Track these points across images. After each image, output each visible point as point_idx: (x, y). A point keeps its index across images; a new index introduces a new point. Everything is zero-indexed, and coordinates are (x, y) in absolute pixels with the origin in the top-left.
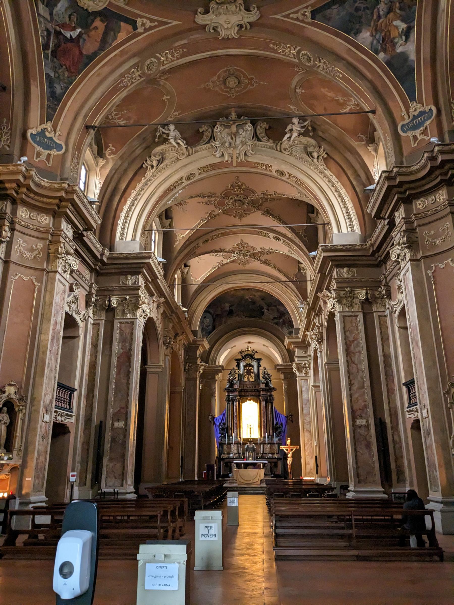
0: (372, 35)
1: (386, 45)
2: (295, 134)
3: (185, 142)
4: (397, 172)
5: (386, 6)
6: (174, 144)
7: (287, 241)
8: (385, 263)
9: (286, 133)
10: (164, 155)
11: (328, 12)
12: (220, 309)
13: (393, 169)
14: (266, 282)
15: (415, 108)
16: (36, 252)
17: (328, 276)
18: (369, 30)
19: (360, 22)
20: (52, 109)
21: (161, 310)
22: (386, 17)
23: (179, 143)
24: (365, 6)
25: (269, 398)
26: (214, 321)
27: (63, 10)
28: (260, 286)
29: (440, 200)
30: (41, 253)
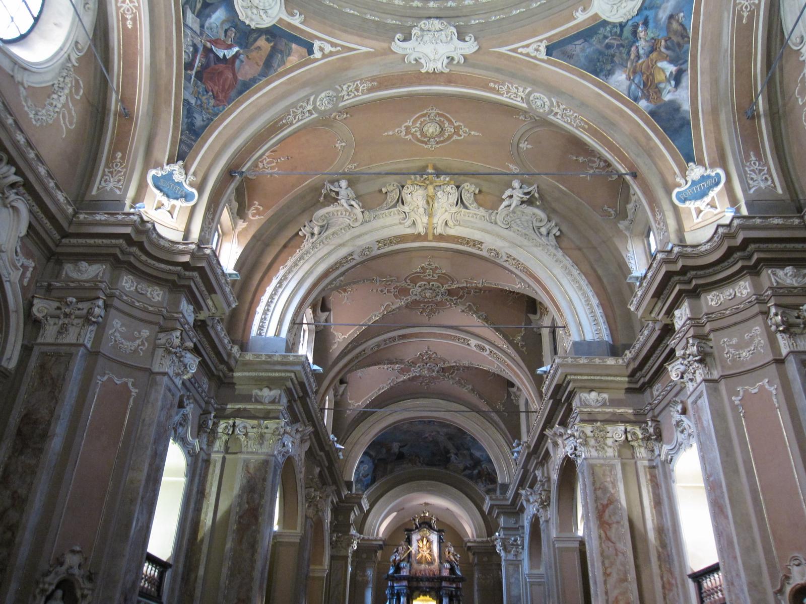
0: (629, 79)
1: (648, 92)
2: (515, 202)
3: (361, 204)
4: (678, 252)
5: (648, 44)
6: (345, 205)
7: (495, 351)
8: (651, 387)
9: (503, 200)
10: (330, 220)
11: (569, 48)
12: (384, 451)
13: (672, 248)
14: (456, 412)
15: (696, 172)
16: (138, 342)
17: (564, 403)
18: (625, 72)
19: (612, 62)
20: (186, 144)
21: (306, 446)
22: (648, 56)
23: (352, 206)
24: (619, 43)
25: (454, 593)
26: (374, 471)
27: (218, 24)
28: (447, 416)
29: (742, 294)
30: (146, 344)
